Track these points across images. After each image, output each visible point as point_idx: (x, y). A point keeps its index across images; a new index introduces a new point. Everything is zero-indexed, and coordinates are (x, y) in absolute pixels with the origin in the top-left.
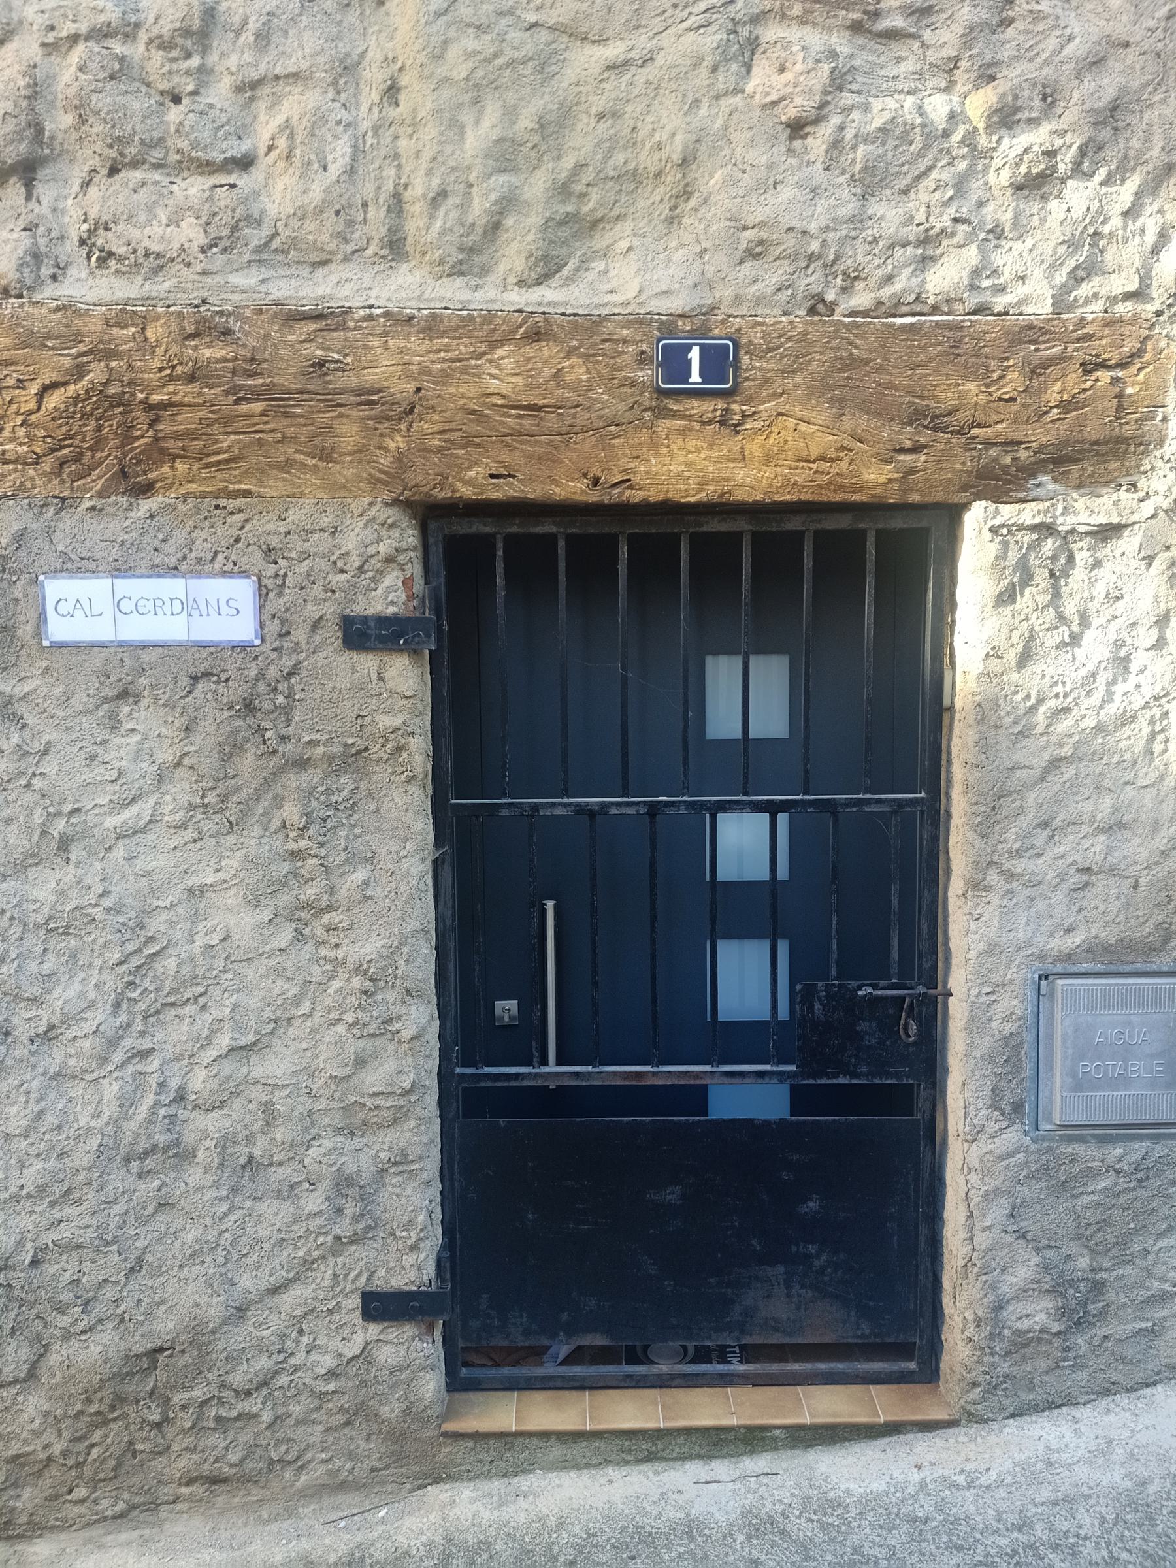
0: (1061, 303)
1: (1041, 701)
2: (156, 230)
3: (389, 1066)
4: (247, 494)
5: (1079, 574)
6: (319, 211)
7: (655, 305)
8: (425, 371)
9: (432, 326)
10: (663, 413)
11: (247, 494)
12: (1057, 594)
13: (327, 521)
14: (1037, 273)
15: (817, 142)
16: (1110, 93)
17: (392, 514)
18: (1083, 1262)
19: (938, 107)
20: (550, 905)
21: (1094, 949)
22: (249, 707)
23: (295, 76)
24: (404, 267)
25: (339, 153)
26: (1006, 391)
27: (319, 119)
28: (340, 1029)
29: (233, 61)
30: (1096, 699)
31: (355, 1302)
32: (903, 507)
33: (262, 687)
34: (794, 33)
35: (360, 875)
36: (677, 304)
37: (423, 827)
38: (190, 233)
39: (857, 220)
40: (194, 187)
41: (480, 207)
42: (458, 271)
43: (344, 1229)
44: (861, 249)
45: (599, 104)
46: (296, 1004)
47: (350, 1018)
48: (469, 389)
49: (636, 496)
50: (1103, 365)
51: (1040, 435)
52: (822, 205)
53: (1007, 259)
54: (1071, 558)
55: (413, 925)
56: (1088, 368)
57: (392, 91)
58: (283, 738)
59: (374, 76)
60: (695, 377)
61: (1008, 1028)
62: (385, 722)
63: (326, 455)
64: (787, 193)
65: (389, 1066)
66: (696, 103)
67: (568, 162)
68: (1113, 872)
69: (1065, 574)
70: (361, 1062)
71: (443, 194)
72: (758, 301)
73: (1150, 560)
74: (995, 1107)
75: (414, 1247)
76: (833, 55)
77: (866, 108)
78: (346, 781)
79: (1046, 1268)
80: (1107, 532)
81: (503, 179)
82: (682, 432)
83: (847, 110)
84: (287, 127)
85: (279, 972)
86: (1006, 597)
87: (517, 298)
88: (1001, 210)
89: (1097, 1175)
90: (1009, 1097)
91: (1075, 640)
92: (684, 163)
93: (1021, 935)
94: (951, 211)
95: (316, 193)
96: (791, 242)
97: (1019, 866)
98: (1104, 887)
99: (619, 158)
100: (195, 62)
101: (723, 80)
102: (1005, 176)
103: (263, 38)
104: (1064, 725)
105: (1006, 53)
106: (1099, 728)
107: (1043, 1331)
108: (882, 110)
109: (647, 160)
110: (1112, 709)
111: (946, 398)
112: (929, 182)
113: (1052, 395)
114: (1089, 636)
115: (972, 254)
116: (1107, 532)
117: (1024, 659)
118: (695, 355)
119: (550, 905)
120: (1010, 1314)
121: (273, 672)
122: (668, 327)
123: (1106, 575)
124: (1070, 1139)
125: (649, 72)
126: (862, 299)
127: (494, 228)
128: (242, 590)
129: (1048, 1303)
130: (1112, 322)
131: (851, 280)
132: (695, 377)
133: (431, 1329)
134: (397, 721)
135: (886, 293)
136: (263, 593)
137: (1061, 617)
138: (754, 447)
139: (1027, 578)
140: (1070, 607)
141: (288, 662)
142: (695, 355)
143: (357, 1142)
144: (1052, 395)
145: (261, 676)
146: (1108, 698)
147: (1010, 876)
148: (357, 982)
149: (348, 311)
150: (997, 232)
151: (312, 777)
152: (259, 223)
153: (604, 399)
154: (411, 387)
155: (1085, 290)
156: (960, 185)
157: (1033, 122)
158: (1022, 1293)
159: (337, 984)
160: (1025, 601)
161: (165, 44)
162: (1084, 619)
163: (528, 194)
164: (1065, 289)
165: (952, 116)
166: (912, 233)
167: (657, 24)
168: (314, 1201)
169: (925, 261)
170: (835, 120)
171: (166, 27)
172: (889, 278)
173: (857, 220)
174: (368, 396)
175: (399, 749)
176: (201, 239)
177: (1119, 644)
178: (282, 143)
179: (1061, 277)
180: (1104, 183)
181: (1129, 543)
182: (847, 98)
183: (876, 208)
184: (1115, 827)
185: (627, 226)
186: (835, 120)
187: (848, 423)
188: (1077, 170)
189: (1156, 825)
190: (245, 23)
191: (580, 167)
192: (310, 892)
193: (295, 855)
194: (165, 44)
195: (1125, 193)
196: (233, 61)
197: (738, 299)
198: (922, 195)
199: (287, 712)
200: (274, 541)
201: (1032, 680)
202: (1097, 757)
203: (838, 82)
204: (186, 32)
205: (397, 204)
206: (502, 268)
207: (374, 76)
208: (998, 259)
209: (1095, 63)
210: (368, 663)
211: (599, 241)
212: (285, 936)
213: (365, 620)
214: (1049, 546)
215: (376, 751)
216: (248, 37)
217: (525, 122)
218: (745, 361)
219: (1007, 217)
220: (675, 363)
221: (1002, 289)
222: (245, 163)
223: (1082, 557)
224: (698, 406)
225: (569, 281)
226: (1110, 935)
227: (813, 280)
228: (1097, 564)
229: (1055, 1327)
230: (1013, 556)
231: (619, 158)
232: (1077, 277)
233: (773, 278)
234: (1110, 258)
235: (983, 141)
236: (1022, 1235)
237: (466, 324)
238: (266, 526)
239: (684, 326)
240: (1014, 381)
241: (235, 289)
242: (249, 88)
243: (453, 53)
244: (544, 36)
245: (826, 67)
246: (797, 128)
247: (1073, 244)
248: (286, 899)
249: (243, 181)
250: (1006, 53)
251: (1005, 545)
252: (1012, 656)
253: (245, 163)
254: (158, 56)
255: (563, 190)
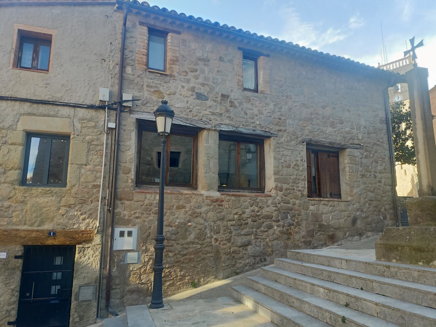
0: (85, 229)
1: (81, 262)
2: (2, 223)
3: (13, 299)
4: (7, 245)
5: (86, 251)
6: (18, 221)
7: (49, 229)
8: (26, 234)
9: (28, 231)
10: (48, 238)
11: (7, 245)
12: (84, 253)
13: (15, 247)
14: (83, 226)
15: (65, 216)
16: (90, 213)
17: (22, 246)
18: (82, 314)
19: (76, 213)
20: (34, 283)
21: (85, 284)
22: (4, 264)
23: (17, 210)
24: (26, 226)
25: (21, 217)
26: (80, 236)
27: (19, 214)
28: (9, 295)
29: (12, 209)
30: (87, 261)
31: (7, 323)
32: (70, 245)
33: (6, 262)
34: (63, 208)
35: (13, 280)
36: (51, 229)
37: (20, 275)
38: (5, 223)
39: (68, 222)
40: (6, 219)
41: (33, 221)
42: (31, 226)
43: (6, 315)
44: (68, 224)
45: (45, 213)
46: (4, 293)
47: (10, 294)
48: (30, 236)
49: (45, 245)
50: (89, 234)
51: (83, 239)
52: (65, 221)
53: (81, 225)
54: (85, 250)
55: (18, 285)
56: (87, 234)
57: (26, 212)
58: (7, 267)
59: (25, 211)
60: (52, 235)
61: (76, 292)
62: (18, 265)
63: (16, 242)
64: (62, 220)
65: (13, 299)
66: (54, 213)
67: (42, 217)
68: (87, 277)
69: (85, 251)
70: (10, 298)
71: (30, 220)
72: (58, 228)
73: (92, 250)
74: (75, 299)
75: (14, 317)
76: (67, 210)
77: (69, 214)
78: (13, 271)
79: (78, 315)
80: (88, 247)
81: (36, 219)
82: (50, 239)
83: (67, 214)
84: (16, 215)
85: (3, 290)
86: (79, 253)
87: (36, 228)
88: (81, 221)
89: (83, 305)
90: (76, 298)
91: (85, 257)
92: (53, 218)
93: (78, 283)
94: (76, 222)
95: (18, 220)
96: (62, 224)
97: (78, 277)
98: (86, 278)
99: (47, 217)
100: (8, 209)
101: (57, 211)
102: (81, 219)
103: (15, 208)
104: (84, 264)
105: (82, 209)
106: (87, 264)
107: (78, 321)
108: (71, 214)
109: (49, 217)
110: (88, 262)
111: (75, 236)
112: (74, 219)
113: (84, 236)
114: (86, 256)
115: (78, 225)
116: (88, 247)
117: (80, 258)
118: (52, 233)
119: (34, 283)
120: (75, 320)
121: (7, 261)
122: (50, 231)
123: (88, 251)
124: (81, 302)
125: (50, 211)
126: (68, 228)
127: (35, 222)
128: (5, 254)
129: (78, 318)
130: (90, 230)
131: (67, 227)
132: (52, 235)
133: (14, 326)
134: (19, 265)
135: (70, 228)
136: (7, 254)
137: (84, 255)
138: (57, 240)
139: (81, 251)
140: (85, 254)
141: (8, 260)
142: (52, 233)
143: (9, 307)
144: (84, 236)
145: (6, 261)
146: (88, 261)
147: (78, 278)
148: (11, 290)
149: (20, 229)
150: (80, 223)
151: (9, 271)
152: (12, 222)
153: (44, 237)
154: (25, 236)
155: (88, 228)
156: (77, 220)
157: (84, 215)
158: (76, 318)
159: (9, 291)
160: (81, 253)
161: (5, 208)
162: (86, 255)
163: (377, 184)
164: (86, 228)
165: (77, 214)
166: (73, 223)
167: (51, 207)
168: (4, 313)
169: (74, 225)
170: (66, 215)
171: (6, 207)
172: (70, 227)
173: (68, 222)
174: (21, 236)
175: (19, 268)
176: (6, 224)
177: (89, 257)
178: (15, 216)
179: (85, 227)
180: (90, 219)
181: (90, 248)
182: (68, 213)
183: (70, 221)
184: (87, 273)
185: (47, 222)
186: (66, 215)
187: (66, 239)
188: (87, 218)
189: (91, 273)
190: (13, 206)
191: (43, 218)
192: (7, 282)
193: (7, 278)
194: (5, 208)
195: (91, 220)
196: (12, 209)
197: (56, 228)
198: (74, 220)
199: (8, 265)
200: (9, 249)
201: (81, 260)
202: (86, 267)
203: (67, 212)
204: (8, 207)
205: (26, 220)
206: (35, 225)
207: (25, 211)
208: (80, 225)
209: (89, 210)
210: (17, 260)
211: (44, 223)
212: (4, 286)
213: (17, 256)
214: (83, 249)
215: (16, 268)
216: (14, 207)
217: (38, 214)
218: (57, 233)
219: (81, 222)
220: (50, 234)
221: (81, 228)
222: (12, 217)
223: (86, 250)
224: (52, 237)
225: (41, 227)
226: (86, 283)
227: (63, 227)
228: (87, 250)
229: (79, 321)
230: (80, 250)
231: (47, 217)
232: (87, 227)
233: (60, 227)
234: (90, 225)
235: (79, 216)
236: (76, 312)
237: (31, 231)
238: (9, 248)
239: (51, 230)
240: (81, 235)
241: (9, 228)
242: (13, 211)
243: (33, 209)
244: (41, 207)
245: (66, 211)
246: (63, 215)
247: (87, 224)
248: (5, 282)
249: (11, 219)
250: (82, 209)
251: (79, 249)
252: (79, 258)
253: (12, 217)
254: (5, 209)
255: (41, 219)
